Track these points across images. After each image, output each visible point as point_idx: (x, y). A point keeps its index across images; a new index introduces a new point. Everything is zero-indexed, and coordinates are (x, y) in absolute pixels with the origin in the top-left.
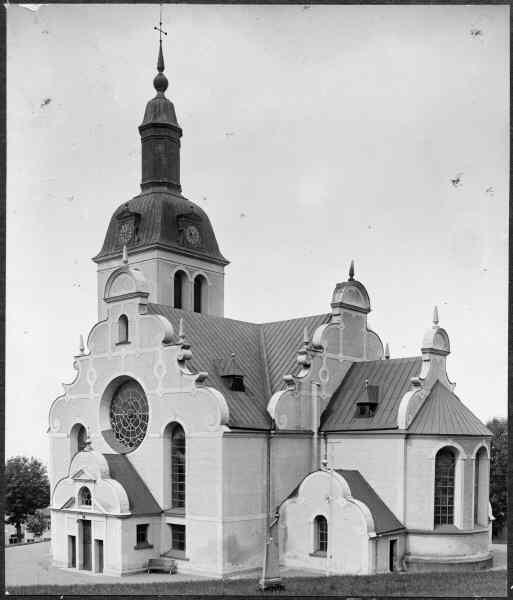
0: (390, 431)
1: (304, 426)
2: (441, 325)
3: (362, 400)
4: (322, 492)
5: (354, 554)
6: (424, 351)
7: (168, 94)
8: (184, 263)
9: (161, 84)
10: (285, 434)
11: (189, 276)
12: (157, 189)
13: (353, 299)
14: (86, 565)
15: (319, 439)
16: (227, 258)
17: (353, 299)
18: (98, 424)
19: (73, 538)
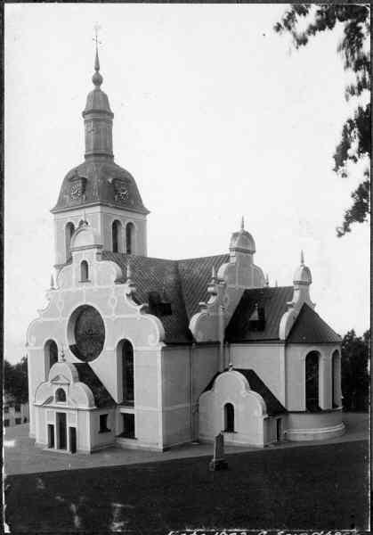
0: (276, 340)
1: (214, 340)
2: (306, 264)
3: (253, 314)
4: (232, 387)
5: (252, 431)
6: (295, 283)
7: (103, 87)
8: (118, 215)
9: (98, 81)
10: (201, 345)
11: (122, 223)
12: (98, 158)
13: (245, 243)
14: (62, 446)
15: (224, 347)
16: (149, 210)
17: (245, 243)
18: (65, 343)
19: (51, 427)
